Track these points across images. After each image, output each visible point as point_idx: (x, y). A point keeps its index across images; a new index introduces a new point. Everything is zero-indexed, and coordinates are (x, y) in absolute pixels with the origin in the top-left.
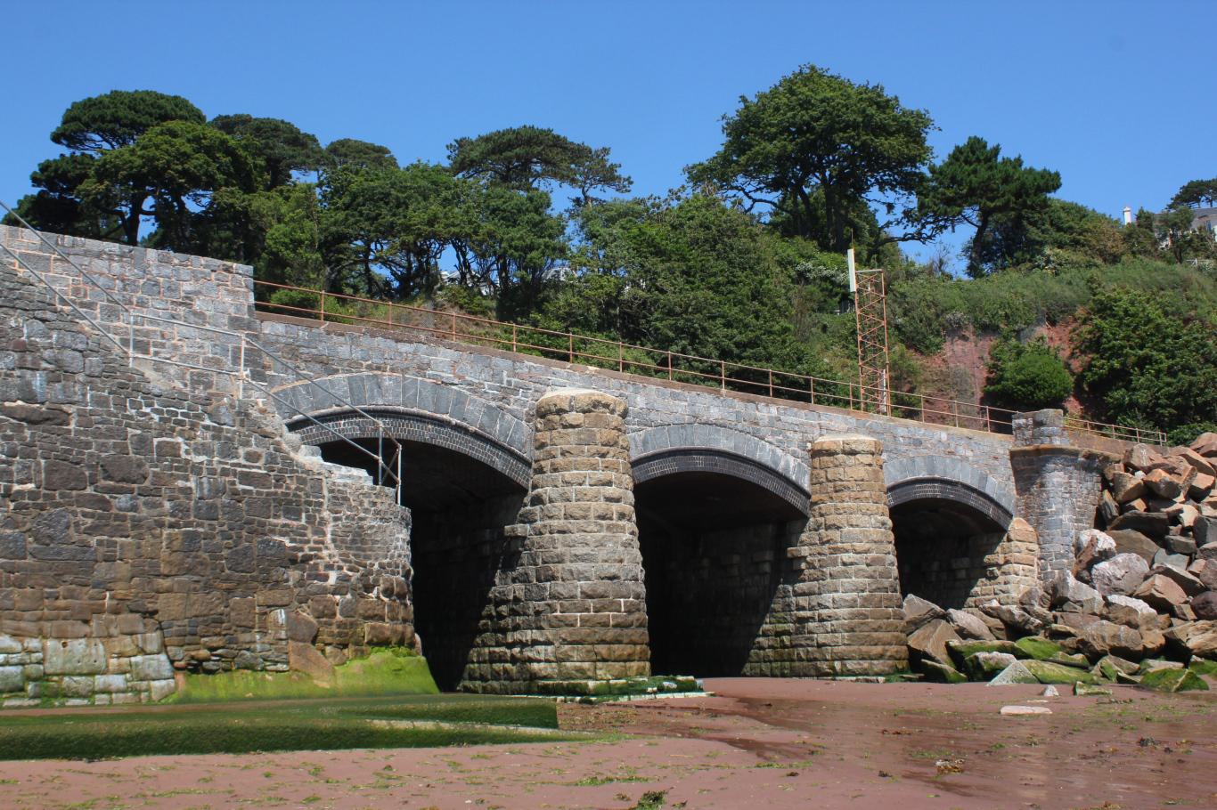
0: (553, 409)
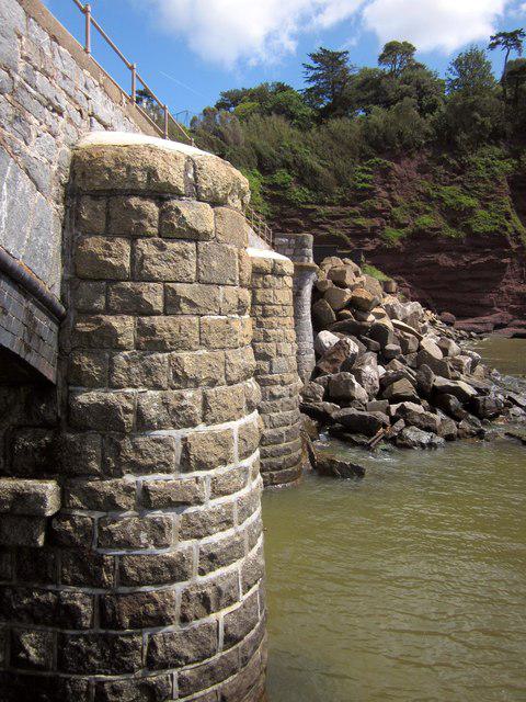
0: (141, 178)
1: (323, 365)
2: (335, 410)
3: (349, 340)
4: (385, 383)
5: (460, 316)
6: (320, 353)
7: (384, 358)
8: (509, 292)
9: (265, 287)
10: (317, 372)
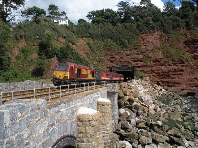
1: (121, 118)
2: (122, 132)
3: (128, 112)
4: (137, 123)
5: (169, 86)
6: (120, 115)
7: (138, 115)
8: (185, 78)
9: (104, 108)
10: (119, 121)
